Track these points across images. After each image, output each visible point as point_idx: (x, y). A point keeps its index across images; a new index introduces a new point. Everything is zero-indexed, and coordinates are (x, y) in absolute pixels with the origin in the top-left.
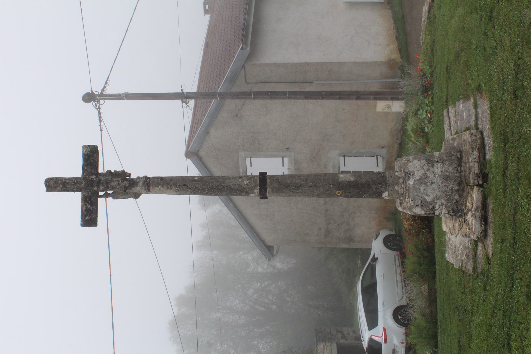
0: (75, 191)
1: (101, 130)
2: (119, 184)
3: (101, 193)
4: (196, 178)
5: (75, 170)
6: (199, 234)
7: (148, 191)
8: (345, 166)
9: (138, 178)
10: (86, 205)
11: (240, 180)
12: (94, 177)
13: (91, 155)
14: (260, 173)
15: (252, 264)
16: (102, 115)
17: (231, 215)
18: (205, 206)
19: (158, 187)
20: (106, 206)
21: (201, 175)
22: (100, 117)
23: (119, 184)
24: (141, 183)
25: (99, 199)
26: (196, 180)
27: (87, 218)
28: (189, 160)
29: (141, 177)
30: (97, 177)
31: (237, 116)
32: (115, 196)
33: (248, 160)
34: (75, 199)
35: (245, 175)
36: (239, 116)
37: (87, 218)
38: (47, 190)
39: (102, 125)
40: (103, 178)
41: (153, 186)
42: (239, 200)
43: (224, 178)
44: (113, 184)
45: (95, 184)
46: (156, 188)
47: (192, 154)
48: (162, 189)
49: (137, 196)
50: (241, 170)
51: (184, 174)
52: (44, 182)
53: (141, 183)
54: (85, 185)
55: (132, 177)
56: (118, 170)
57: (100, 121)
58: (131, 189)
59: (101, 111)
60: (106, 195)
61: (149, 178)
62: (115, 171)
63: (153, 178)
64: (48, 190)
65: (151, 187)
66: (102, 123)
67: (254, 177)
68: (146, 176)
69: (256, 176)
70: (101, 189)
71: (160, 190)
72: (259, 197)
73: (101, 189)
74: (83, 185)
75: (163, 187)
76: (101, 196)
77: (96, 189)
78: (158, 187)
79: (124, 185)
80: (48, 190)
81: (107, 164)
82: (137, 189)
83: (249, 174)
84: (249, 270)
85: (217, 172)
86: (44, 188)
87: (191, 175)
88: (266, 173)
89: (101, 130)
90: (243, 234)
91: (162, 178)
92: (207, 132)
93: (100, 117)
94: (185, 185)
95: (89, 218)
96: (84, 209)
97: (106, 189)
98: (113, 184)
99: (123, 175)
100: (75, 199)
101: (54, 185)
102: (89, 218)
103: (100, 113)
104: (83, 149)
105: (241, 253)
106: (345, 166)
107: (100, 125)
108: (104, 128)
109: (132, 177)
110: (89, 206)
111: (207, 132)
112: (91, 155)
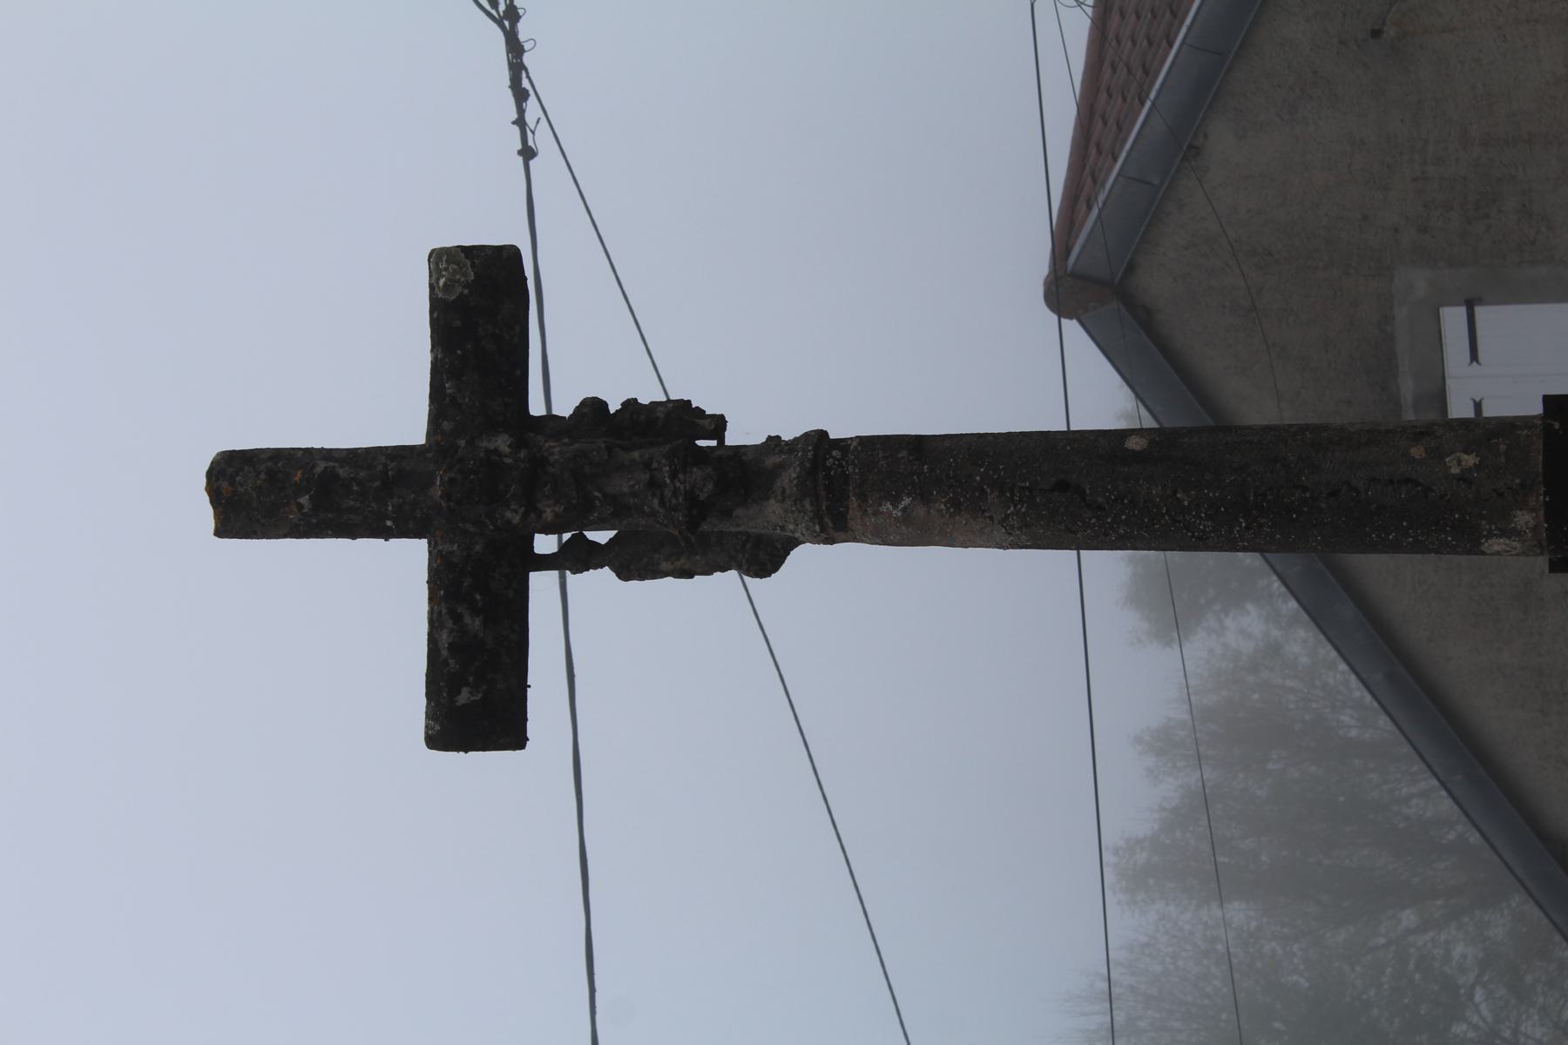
0: (387, 534)
2: (654, 485)
3: (545, 544)
4: (1134, 444)
5: (384, 400)
6: (1139, 799)
7: (833, 528)
8: (1474, 357)
9: (774, 441)
10: (457, 618)
11: (1417, 452)
12: (502, 443)
13: (481, 303)
14: (1548, 400)
15: (1479, 995)
16: (527, 59)
17: (1339, 674)
18: (1172, 617)
19: (895, 501)
21: (1149, 422)
22: (517, 69)
23: (654, 485)
24: (788, 479)
26: (1136, 456)
27: (464, 697)
28: (1072, 327)
29: (787, 437)
30: (519, 444)
31: (1376, 34)
32: (633, 562)
33: (1453, 319)
34: (388, 578)
35: (1432, 416)
36: (1390, 32)
37: (464, 697)
38: (222, 531)
39: (530, 118)
40: (556, 450)
41: (863, 497)
42: (1398, 578)
43: (1316, 440)
44: (621, 485)
45: (511, 491)
47: (1090, 284)
48: (921, 511)
49: (763, 558)
50: (1407, 388)
52: (203, 481)
54: (447, 496)
55: (731, 439)
57: (521, 96)
58: (727, 514)
59: (524, 31)
60: (578, 557)
61: (841, 444)
62: (631, 405)
63: (868, 443)
64: (224, 529)
65: (854, 502)
66: (532, 106)
67: (1507, 426)
68: (822, 434)
69: (1526, 421)
70: (548, 515)
71: (907, 517)
72: (1542, 562)
73: (548, 515)
74: (436, 492)
75: (924, 498)
76: (545, 563)
77: (516, 519)
78: (895, 501)
79: (691, 495)
80: (224, 529)
81: (578, 362)
82: (773, 514)
83: (1459, 408)
84: (1459, 1029)
85: (1257, 403)
86: (206, 514)
87: (1084, 421)
89: (528, 153)
90: (1422, 797)
91: (917, 444)
92: (1182, 146)
93: (517, 69)
94: (1063, 486)
95: (477, 696)
96: (444, 638)
97: (574, 517)
98: (621, 485)
99: (676, 426)
100: (388, 578)
101: (265, 493)
102: (477, 696)
103: (515, 48)
104: (435, 272)
105: (1409, 918)
106: (1474, 357)
107: (521, 122)
108: (541, 139)
109: (731, 439)
110: (474, 623)
111: (1182, 146)
112: (481, 303)
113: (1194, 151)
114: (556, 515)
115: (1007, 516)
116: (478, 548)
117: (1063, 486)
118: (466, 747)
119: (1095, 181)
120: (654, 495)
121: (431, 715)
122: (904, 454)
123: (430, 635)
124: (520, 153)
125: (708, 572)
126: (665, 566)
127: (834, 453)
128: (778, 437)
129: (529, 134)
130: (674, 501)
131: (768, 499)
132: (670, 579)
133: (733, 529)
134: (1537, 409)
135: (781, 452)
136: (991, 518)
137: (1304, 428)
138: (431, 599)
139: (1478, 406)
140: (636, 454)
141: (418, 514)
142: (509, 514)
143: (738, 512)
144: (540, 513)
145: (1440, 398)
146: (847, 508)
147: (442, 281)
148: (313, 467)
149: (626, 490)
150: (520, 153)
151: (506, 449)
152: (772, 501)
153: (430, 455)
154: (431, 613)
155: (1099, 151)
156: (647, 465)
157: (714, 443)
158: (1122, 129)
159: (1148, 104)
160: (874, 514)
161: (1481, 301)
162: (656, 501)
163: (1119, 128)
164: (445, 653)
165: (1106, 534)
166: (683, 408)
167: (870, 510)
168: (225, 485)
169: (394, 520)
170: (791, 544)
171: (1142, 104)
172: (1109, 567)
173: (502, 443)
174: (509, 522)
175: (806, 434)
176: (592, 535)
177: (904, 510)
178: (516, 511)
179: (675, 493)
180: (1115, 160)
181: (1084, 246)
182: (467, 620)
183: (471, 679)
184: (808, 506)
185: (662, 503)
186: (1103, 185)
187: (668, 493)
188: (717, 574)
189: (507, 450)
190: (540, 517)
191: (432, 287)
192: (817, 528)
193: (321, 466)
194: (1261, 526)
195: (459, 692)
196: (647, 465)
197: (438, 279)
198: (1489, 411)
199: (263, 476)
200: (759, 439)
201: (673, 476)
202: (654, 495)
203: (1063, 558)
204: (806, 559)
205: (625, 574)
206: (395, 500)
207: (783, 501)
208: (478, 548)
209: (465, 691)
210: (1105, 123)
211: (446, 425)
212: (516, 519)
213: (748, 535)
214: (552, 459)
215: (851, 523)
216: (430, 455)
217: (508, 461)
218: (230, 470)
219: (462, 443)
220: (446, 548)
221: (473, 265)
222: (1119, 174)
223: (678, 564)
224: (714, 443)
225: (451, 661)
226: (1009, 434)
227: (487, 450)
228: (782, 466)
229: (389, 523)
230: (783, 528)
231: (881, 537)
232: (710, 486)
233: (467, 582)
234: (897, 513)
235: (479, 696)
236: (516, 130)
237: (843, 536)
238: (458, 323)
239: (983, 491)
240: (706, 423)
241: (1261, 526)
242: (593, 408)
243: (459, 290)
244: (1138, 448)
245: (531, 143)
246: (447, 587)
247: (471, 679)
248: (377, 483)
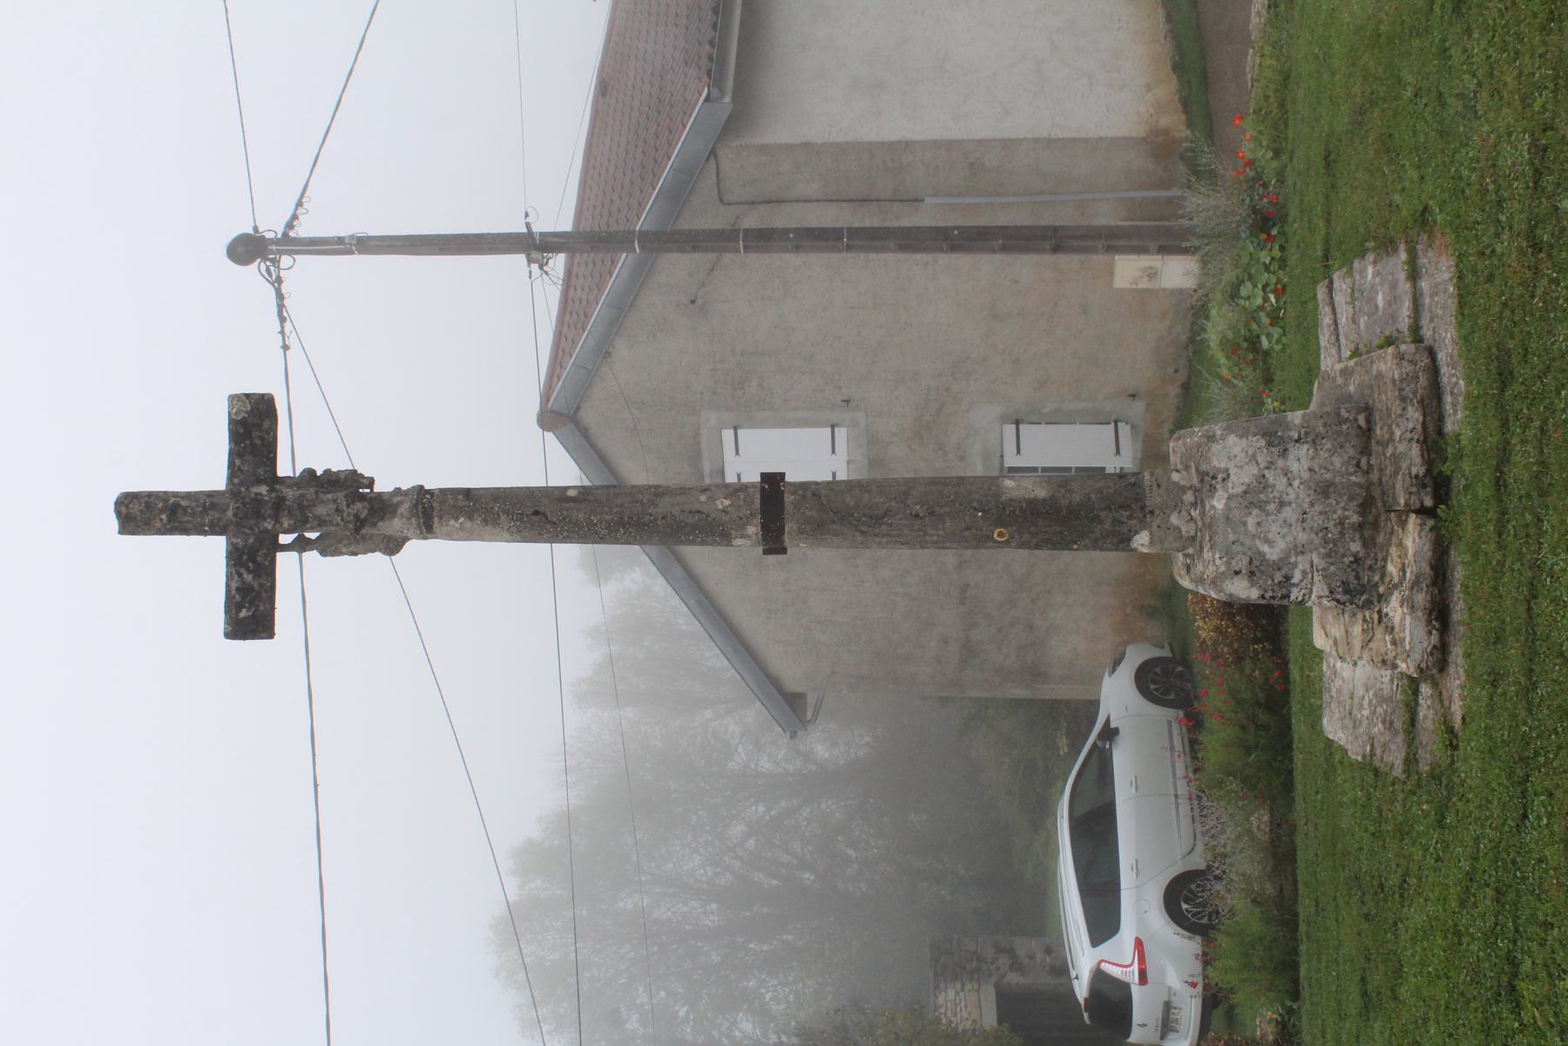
0: (205, 533)
2: (338, 510)
3: (285, 539)
4: (571, 493)
5: (205, 467)
6: (583, 659)
8: (737, 453)
9: (398, 491)
10: (240, 575)
11: (703, 498)
12: (263, 489)
13: (254, 425)
14: (763, 475)
15: (740, 749)
18: (599, 575)
19: (457, 519)
21: (587, 483)
22: (281, 306)
25: (281, 557)
26: (573, 500)
27: (243, 613)
28: (550, 436)
29: (404, 488)
30: (272, 490)
31: (693, 302)
32: (328, 547)
33: (728, 435)
34: (204, 559)
35: (718, 481)
36: (699, 301)
37: (243, 613)
39: (287, 330)
40: (290, 494)
41: (441, 517)
42: (699, 555)
44: (321, 510)
45: (267, 511)
46: (452, 522)
47: (560, 417)
48: (469, 524)
49: (392, 546)
50: (707, 467)
51: (537, 481)
54: (235, 515)
55: (376, 489)
56: (334, 470)
57: (282, 320)
58: (375, 525)
59: (284, 289)
60: (301, 545)
61: (428, 492)
62: (327, 472)
63: (443, 492)
65: (436, 520)
69: (753, 485)
70: (286, 525)
71: (462, 528)
73: (286, 525)
74: (230, 513)
75: (470, 518)
78: (457, 519)
79: (356, 514)
81: (301, 450)
82: (394, 526)
83: (731, 478)
85: (637, 473)
87: (556, 481)
88: (782, 475)
89: (285, 348)
90: (712, 657)
91: (467, 493)
92: (603, 352)
93: (281, 306)
94: (536, 513)
95: (250, 613)
96: (234, 585)
97: (300, 525)
99: (349, 484)
100: (204, 559)
101: (143, 513)
102: (250, 613)
103: (280, 296)
104: (231, 406)
105: (709, 714)
106: (737, 453)
107: (282, 332)
109: (376, 489)
110: (249, 578)
111: (603, 352)
112: (254, 425)
113: (608, 354)
117: (536, 513)
118: (244, 638)
121: (227, 623)
134: (758, 479)
137: (650, 487)
139: (739, 476)
145: (722, 472)
156: (335, 501)
158: (574, 343)
161: (1023, 422)
170: (405, 540)
172: (569, 553)
176: (307, 535)
193: (172, 500)
196: (335, 501)
198: (744, 480)
200: (391, 489)
203: (542, 548)
205: (324, 553)
220: (235, 540)
226: (529, 488)
228: (401, 502)
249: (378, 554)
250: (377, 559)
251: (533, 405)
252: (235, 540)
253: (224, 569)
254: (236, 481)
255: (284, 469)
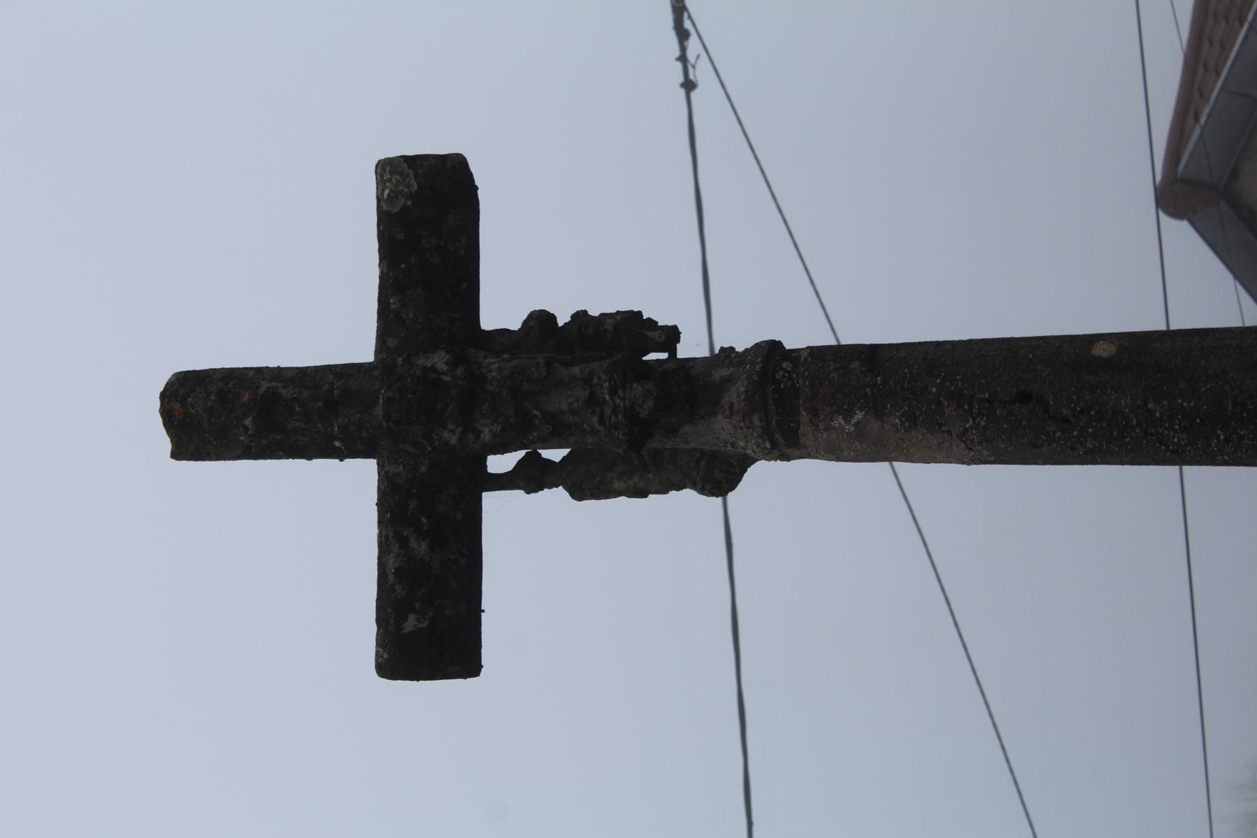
1: (689, 86)
2: (593, 401)
3: (500, 464)
4: (1101, 350)
5: (332, 319)
7: (786, 446)
10: (403, 542)
12: (439, 360)
13: (429, 213)
19: (848, 415)
20: (529, 537)
23: (593, 401)
24: (736, 394)
25: (492, 502)
27: (410, 624)
28: (1181, 233)
32: (586, 481)
34: (334, 505)
37: (410, 624)
39: (691, 55)
40: (492, 366)
41: (813, 412)
44: (560, 402)
45: (458, 407)
46: (839, 421)
48: (874, 426)
49: (718, 477)
51: (1144, 318)
52: (157, 404)
53: (736, 394)
55: (683, 351)
56: (594, 312)
57: (682, 35)
58: (673, 431)
60: (532, 477)
62: (649, 319)
65: (804, 417)
66: (693, 46)
68: (775, 346)
70: (486, 435)
74: (378, 411)
77: (454, 440)
78: (848, 415)
79: (647, 411)
82: (721, 430)
88: (640, 313)
89: (689, 85)
94: (1024, 397)
96: (391, 562)
98: (560, 402)
99: (626, 338)
100: (334, 505)
101: (219, 415)
104: (381, 183)
107: (683, 59)
108: (702, 73)
109: (683, 351)
110: (420, 548)
112: (429, 213)
114: (494, 435)
115: (966, 430)
116: (423, 469)
117: (1024, 397)
119: (1201, 95)
120: (593, 412)
121: (381, 643)
122: (856, 365)
123: (380, 558)
124: (683, 85)
125: (664, 490)
126: (618, 485)
127: (785, 365)
128: (732, 349)
129: (690, 69)
130: (613, 419)
131: (715, 414)
132: (623, 499)
133: (686, 447)
135: (730, 364)
136: (949, 432)
138: (380, 522)
140: (576, 370)
141: (364, 434)
142: (446, 435)
143: (686, 428)
144: (478, 433)
146: (799, 424)
147: (386, 192)
148: (258, 388)
149: (564, 407)
150: (683, 85)
151: (442, 366)
152: (720, 417)
153: (376, 373)
154: (380, 536)
155: (1206, 69)
156: (587, 381)
157: (664, 356)
158: (1225, 47)
159: (1246, 26)
160: (827, 429)
162: (595, 419)
163: (1222, 45)
164: (391, 578)
165: (1073, 449)
166: (633, 319)
167: (821, 426)
168: (177, 406)
169: (342, 440)
171: (1241, 24)
173: (439, 360)
174: (447, 443)
175: (757, 346)
177: (857, 425)
178: (453, 431)
179: (615, 411)
180: (1218, 75)
181: (1191, 155)
182: (413, 544)
183: (417, 605)
184: (757, 423)
185: (601, 421)
186: (1208, 100)
187: (608, 411)
188: (673, 493)
189: (445, 367)
190: (478, 437)
191: (379, 199)
192: (768, 445)
194: (1242, 438)
195: (406, 619)
197: (383, 191)
199: (213, 397)
201: (613, 393)
202: (593, 412)
204: (763, 476)
205: (579, 494)
206: (340, 420)
207: (730, 417)
208: (423, 469)
209: (412, 618)
210: (1211, 43)
211: (391, 342)
212: (454, 440)
213: (703, 452)
214: (489, 377)
215: (803, 439)
216: (376, 373)
217: (447, 378)
218: (182, 392)
219: (400, 361)
220: (392, 469)
221: (416, 175)
222: (1222, 89)
223: (631, 483)
224: (664, 356)
225: (398, 587)
227: (424, 368)
228: (729, 380)
229: (337, 444)
230: (733, 445)
231: (835, 453)
232: (651, 403)
233: (413, 504)
234: (849, 428)
235: (427, 623)
236: (679, 65)
237: (796, 452)
238: (401, 236)
239: (939, 403)
240: (656, 335)
241: (1242, 438)
242: (541, 321)
243: (402, 201)
244: (1105, 355)
245: (691, 77)
246: (397, 510)
247: (417, 605)
248: (320, 403)
249: (689, 494)
250: (686, 505)
251: (1139, 171)
252: (392, 469)
253: (374, 531)
254: (391, 342)
255: (500, 310)
